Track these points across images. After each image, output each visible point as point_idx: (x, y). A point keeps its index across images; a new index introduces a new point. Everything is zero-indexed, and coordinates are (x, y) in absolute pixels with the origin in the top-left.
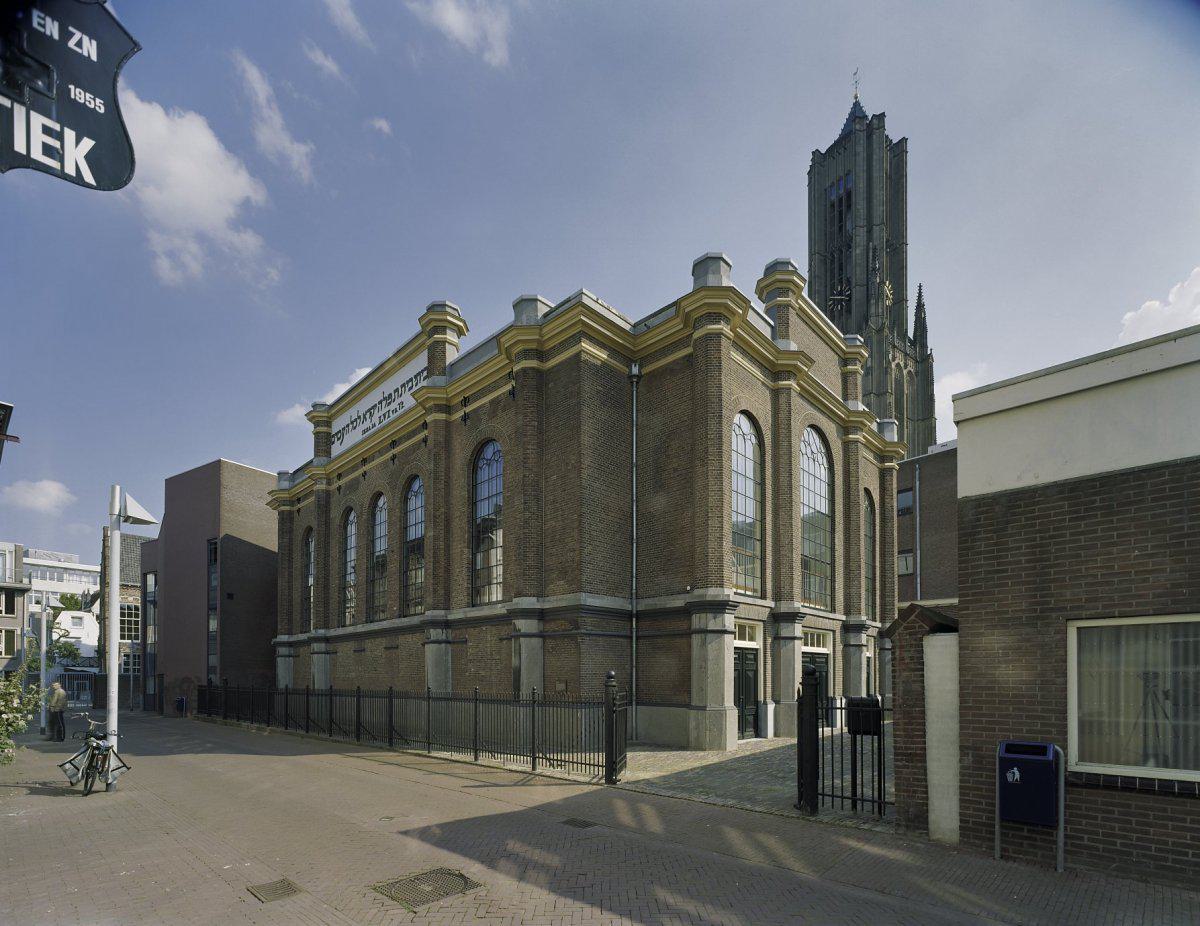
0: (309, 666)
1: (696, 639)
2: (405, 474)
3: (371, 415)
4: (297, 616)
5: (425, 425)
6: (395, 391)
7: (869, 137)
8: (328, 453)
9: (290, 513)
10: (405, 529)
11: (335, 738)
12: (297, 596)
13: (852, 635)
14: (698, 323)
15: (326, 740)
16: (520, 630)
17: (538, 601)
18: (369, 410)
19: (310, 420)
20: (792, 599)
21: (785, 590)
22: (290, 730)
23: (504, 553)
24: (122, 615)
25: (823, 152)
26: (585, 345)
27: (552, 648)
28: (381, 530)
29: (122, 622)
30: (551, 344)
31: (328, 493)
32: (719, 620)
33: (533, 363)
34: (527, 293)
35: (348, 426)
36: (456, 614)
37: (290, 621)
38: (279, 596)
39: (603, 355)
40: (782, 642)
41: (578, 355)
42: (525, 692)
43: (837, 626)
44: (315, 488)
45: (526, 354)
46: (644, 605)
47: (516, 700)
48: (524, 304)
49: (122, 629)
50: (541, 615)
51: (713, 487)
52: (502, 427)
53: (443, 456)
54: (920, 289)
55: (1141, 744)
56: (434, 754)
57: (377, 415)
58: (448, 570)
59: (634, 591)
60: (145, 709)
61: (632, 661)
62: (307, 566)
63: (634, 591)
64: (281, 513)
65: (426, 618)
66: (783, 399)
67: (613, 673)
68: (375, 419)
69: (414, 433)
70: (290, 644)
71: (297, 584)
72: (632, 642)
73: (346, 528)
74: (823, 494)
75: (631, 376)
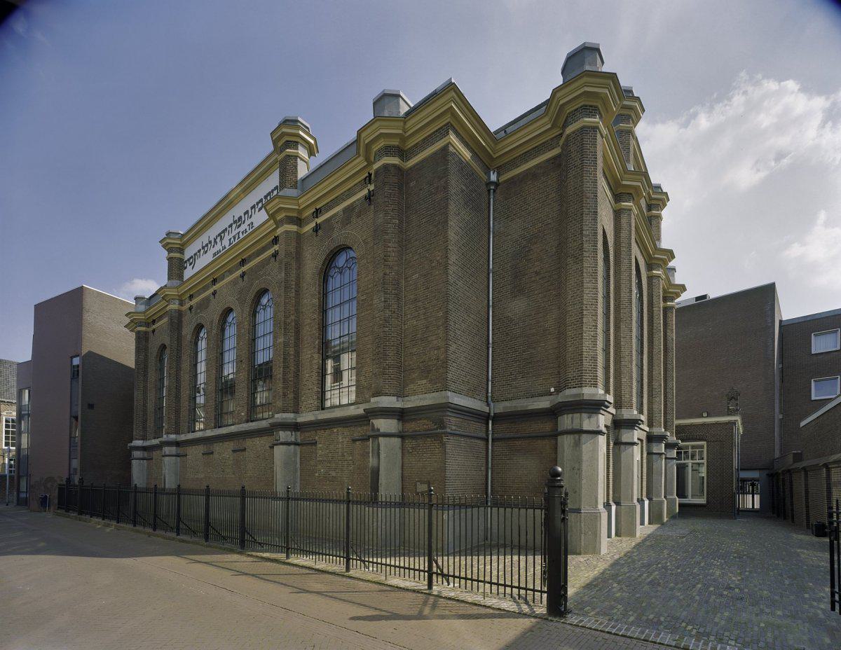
1: (566, 442)
3: (221, 239)
4: (151, 424)
8: (181, 276)
9: (146, 333)
10: (253, 353)
11: (182, 537)
12: (151, 406)
13: (654, 444)
14: (573, 116)
15: (173, 539)
17: (398, 401)
18: (219, 235)
21: (625, 398)
22: (138, 528)
24: (7, 426)
26: (452, 137)
27: (413, 448)
28: (230, 356)
29: (7, 432)
30: (411, 143)
31: (180, 314)
32: (593, 419)
33: (395, 160)
34: (391, 87)
35: (199, 251)
37: (145, 428)
38: (135, 400)
39: (467, 154)
40: (622, 447)
41: (445, 149)
42: (383, 493)
44: (168, 308)
46: (500, 408)
47: (373, 501)
49: (7, 438)
50: (401, 415)
52: (357, 234)
53: (294, 265)
56: (294, 559)
58: (297, 375)
60: (18, 504)
61: (487, 464)
62: (162, 379)
64: (138, 333)
65: (275, 421)
67: (560, 469)
69: (264, 249)
70: (144, 449)
71: (152, 396)
72: (487, 444)
73: (196, 344)
75: (489, 183)
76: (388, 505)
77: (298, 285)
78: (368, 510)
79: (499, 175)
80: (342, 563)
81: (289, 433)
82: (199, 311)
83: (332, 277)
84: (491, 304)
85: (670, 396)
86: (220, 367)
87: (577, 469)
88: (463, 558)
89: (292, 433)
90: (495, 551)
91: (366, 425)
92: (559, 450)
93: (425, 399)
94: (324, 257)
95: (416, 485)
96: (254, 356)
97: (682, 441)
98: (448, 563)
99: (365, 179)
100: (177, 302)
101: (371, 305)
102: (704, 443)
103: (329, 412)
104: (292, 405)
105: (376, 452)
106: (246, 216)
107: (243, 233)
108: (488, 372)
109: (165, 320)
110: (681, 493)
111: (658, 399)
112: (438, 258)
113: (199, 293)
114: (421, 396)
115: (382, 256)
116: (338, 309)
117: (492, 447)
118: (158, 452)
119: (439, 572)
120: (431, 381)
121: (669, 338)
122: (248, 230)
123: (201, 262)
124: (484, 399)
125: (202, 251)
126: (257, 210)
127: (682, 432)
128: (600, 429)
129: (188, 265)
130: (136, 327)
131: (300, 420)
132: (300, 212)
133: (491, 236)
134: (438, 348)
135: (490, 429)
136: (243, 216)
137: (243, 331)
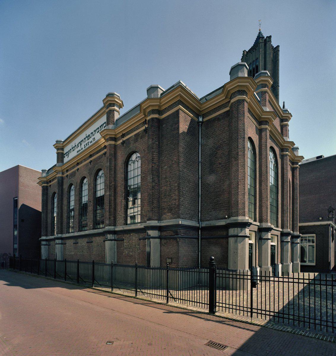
0: (55, 248)
1: (231, 240)
2: (96, 168)
3: (81, 145)
4: (49, 229)
6: (91, 134)
7: (265, 45)
8: (62, 161)
9: (47, 187)
10: (95, 192)
12: (49, 220)
16: (150, 235)
17: (158, 222)
18: (80, 143)
19: (55, 148)
20: (267, 222)
21: (264, 217)
23: (141, 201)
25: (247, 51)
27: (165, 243)
30: (163, 108)
31: (62, 178)
32: (243, 232)
33: (156, 116)
34: (154, 84)
35: (71, 150)
36: (119, 228)
37: (47, 231)
40: (263, 240)
42: (152, 265)
43: (279, 234)
44: (57, 176)
45: (153, 112)
46: (204, 224)
47: (148, 267)
48: (152, 89)
51: (240, 170)
53: (113, 160)
54: (284, 104)
57: (83, 144)
58: (115, 209)
59: (200, 218)
61: (199, 249)
63: (200, 218)
64: (43, 187)
66: (263, 134)
67: (213, 258)
68: (83, 146)
71: (49, 216)
72: (199, 240)
73: (70, 192)
74: (272, 176)
75: (199, 122)
76: (154, 269)
77: (115, 168)
78: (146, 270)
79: (203, 118)
80: (134, 293)
81: (112, 235)
82: (71, 177)
83: (130, 165)
84: (200, 177)
85: (295, 212)
86: (81, 198)
87: (236, 253)
88: (186, 291)
89: (113, 235)
91: (145, 232)
92: (229, 244)
93: (170, 222)
94: (126, 156)
95: (166, 260)
96: (96, 186)
97: (302, 234)
98: (174, 293)
100: (61, 173)
101: (147, 179)
102: (314, 235)
103: (129, 226)
105: (149, 245)
106: (92, 134)
107: (90, 142)
108: (199, 208)
109: (56, 181)
110: (302, 260)
111: (286, 215)
112: (175, 160)
113: (71, 169)
114: (168, 220)
115: (151, 158)
116: (132, 179)
117: (201, 242)
118: (53, 242)
119: (171, 296)
120: (172, 214)
121: (295, 183)
122: (92, 141)
123: (71, 156)
124: (197, 220)
125: (72, 150)
126: (97, 132)
127: (303, 230)
128: (246, 235)
129: (66, 156)
130: (42, 184)
131: (117, 229)
132: (116, 135)
133: (200, 146)
134: (175, 200)
135: (200, 234)
137: (91, 188)
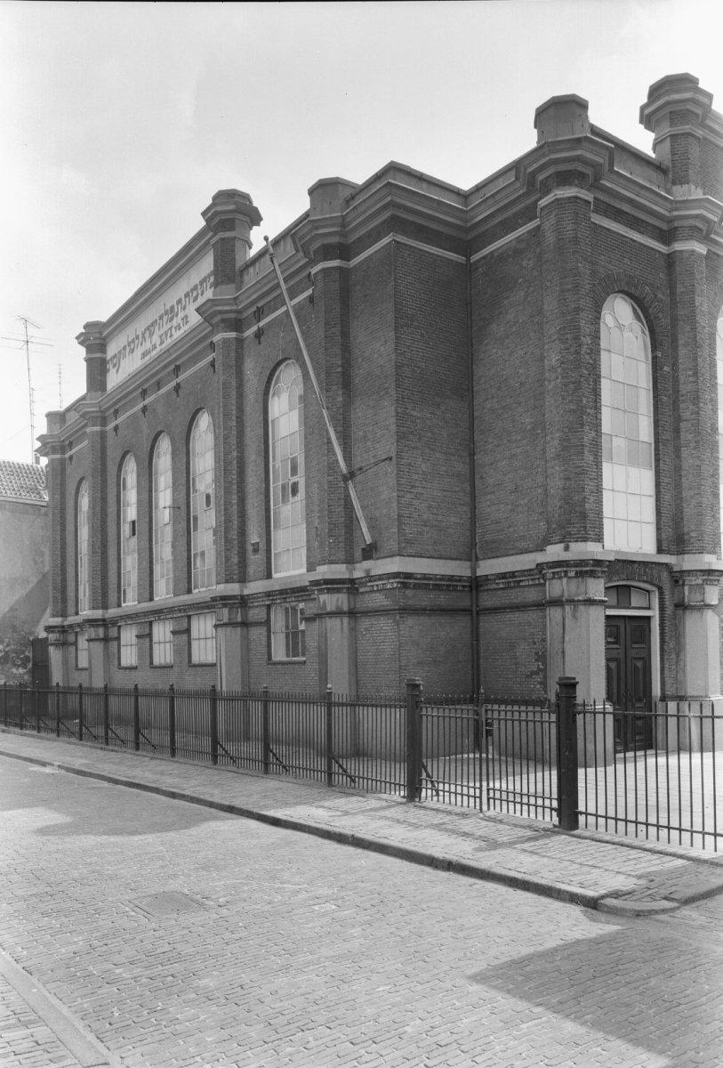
3: (151, 335)
5: (212, 345)
18: (148, 328)
35: (124, 348)
55: (103, 708)
68: (156, 339)
90: (539, 767)
99: (255, 312)
104: (237, 572)
126: (192, 300)
129: (111, 366)
136: (183, 300)
